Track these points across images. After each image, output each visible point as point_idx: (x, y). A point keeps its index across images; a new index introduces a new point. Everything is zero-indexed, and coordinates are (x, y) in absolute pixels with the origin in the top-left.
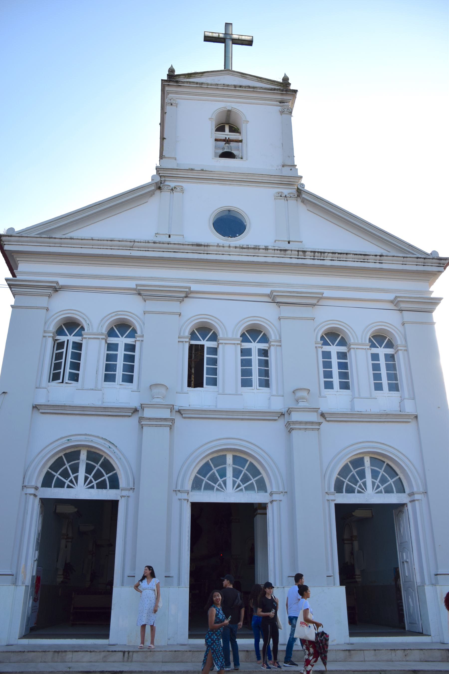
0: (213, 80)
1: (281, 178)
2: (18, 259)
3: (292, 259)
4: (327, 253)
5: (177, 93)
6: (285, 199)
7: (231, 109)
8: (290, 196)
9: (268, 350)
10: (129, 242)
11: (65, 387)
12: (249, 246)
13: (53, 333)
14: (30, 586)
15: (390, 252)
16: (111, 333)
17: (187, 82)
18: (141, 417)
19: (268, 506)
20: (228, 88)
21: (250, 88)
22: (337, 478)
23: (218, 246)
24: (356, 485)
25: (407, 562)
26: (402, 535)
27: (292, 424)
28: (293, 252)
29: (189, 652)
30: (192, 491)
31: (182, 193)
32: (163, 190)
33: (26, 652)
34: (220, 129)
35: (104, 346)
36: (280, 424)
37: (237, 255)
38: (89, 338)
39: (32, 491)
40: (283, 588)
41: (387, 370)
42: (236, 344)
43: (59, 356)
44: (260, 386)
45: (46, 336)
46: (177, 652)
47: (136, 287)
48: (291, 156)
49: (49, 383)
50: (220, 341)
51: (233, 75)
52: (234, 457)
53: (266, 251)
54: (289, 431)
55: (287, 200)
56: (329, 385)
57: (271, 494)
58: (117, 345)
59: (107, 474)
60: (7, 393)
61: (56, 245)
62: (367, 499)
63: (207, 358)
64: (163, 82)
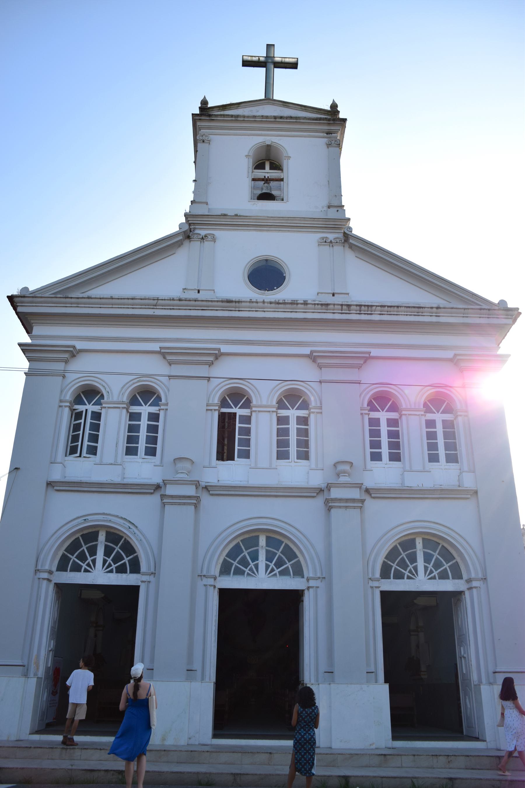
0: (251, 111)
1: (326, 221)
2: (32, 322)
3: (335, 314)
4: (375, 307)
5: (209, 128)
6: (330, 245)
7: (271, 144)
8: (336, 242)
9: (308, 417)
10: (151, 300)
11: (83, 461)
12: (286, 301)
13: (70, 403)
14: (43, 678)
15: (451, 303)
16: (134, 401)
17: (221, 115)
18: (163, 494)
19: (304, 593)
20: (268, 120)
21: (292, 119)
22: (384, 562)
23: (251, 302)
24: (406, 570)
25: (464, 657)
26: (460, 627)
27: (331, 502)
28: (336, 306)
29: (207, 753)
30: (221, 575)
31: (213, 242)
32: (192, 239)
33: (33, 748)
34: (260, 166)
35: (125, 415)
36: (319, 502)
37: (273, 311)
38: (109, 408)
39: (45, 575)
40: (318, 685)
41: (444, 439)
42: (271, 412)
43: (77, 428)
44: (297, 459)
45: (62, 406)
46: (193, 753)
47: (160, 350)
48: (339, 195)
49: (66, 457)
50: (254, 409)
51: (273, 104)
52: (268, 538)
53: (306, 306)
54: (328, 510)
55: (332, 246)
56: (376, 457)
57: (308, 580)
58: (140, 414)
59: (127, 557)
60: (19, 468)
61: (73, 305)
62: (418, 586)
63: (239, 427)
64: (194, 117)
